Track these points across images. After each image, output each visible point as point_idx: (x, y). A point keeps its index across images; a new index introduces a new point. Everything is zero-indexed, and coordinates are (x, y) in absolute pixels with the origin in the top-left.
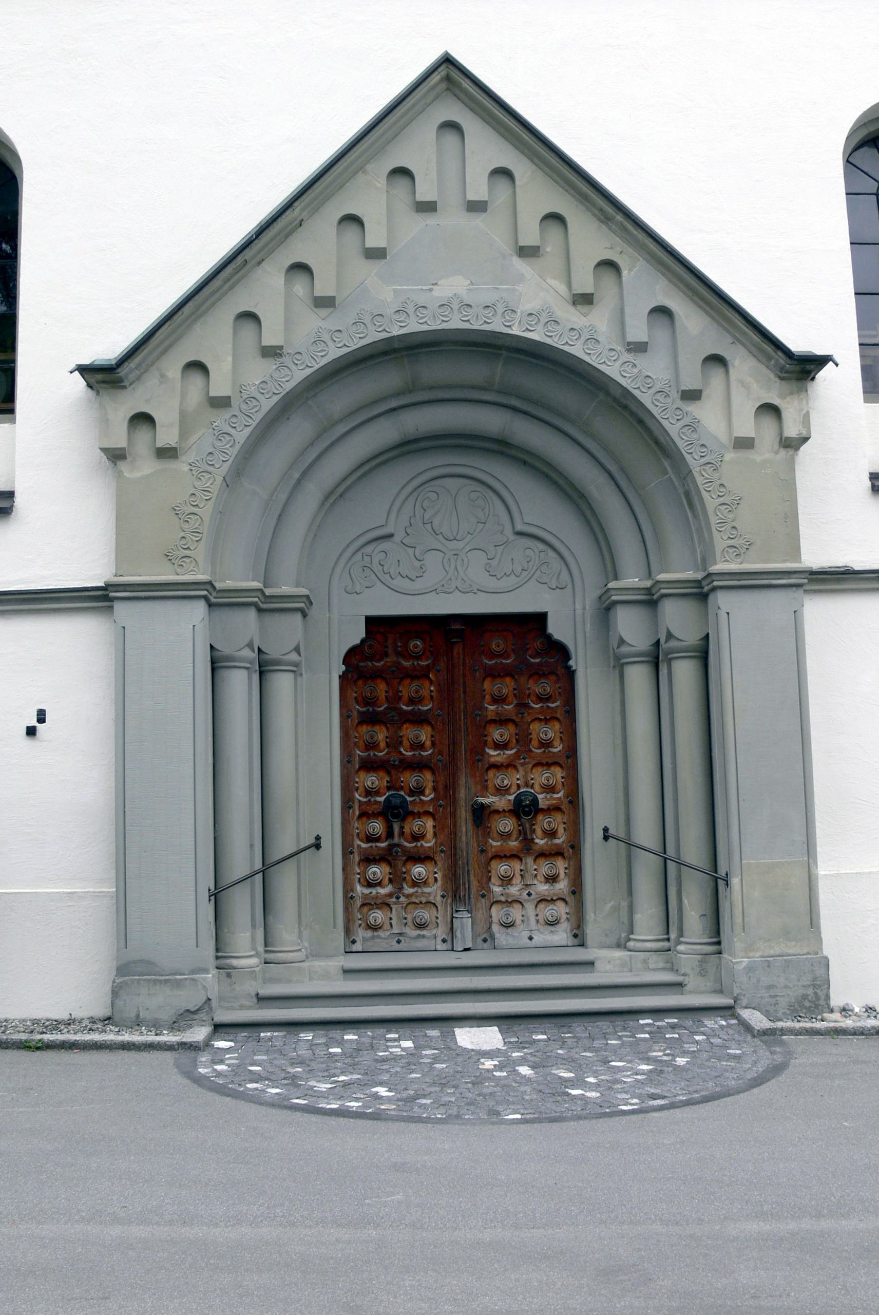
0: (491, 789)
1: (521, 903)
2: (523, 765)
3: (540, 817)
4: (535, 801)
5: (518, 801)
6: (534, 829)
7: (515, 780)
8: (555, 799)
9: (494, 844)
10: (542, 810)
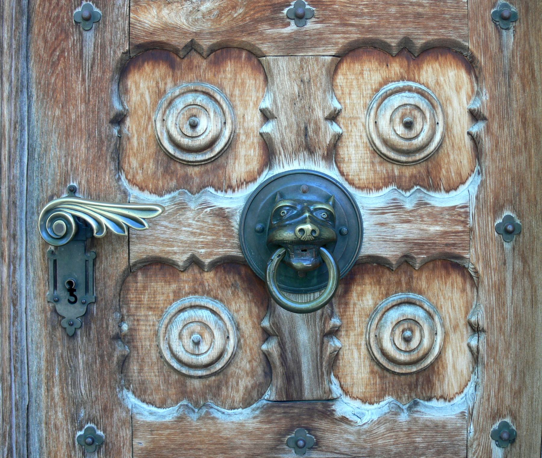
0: (139, 158)
1: (187, 351)
2: (293, 47)
3: (365, 297)
4: (340, 228)
5: (265, 219)
6: (336, 356)
7: (253, 119)
8: (435, 216)
9: (146, 413)
10: (378, 263)
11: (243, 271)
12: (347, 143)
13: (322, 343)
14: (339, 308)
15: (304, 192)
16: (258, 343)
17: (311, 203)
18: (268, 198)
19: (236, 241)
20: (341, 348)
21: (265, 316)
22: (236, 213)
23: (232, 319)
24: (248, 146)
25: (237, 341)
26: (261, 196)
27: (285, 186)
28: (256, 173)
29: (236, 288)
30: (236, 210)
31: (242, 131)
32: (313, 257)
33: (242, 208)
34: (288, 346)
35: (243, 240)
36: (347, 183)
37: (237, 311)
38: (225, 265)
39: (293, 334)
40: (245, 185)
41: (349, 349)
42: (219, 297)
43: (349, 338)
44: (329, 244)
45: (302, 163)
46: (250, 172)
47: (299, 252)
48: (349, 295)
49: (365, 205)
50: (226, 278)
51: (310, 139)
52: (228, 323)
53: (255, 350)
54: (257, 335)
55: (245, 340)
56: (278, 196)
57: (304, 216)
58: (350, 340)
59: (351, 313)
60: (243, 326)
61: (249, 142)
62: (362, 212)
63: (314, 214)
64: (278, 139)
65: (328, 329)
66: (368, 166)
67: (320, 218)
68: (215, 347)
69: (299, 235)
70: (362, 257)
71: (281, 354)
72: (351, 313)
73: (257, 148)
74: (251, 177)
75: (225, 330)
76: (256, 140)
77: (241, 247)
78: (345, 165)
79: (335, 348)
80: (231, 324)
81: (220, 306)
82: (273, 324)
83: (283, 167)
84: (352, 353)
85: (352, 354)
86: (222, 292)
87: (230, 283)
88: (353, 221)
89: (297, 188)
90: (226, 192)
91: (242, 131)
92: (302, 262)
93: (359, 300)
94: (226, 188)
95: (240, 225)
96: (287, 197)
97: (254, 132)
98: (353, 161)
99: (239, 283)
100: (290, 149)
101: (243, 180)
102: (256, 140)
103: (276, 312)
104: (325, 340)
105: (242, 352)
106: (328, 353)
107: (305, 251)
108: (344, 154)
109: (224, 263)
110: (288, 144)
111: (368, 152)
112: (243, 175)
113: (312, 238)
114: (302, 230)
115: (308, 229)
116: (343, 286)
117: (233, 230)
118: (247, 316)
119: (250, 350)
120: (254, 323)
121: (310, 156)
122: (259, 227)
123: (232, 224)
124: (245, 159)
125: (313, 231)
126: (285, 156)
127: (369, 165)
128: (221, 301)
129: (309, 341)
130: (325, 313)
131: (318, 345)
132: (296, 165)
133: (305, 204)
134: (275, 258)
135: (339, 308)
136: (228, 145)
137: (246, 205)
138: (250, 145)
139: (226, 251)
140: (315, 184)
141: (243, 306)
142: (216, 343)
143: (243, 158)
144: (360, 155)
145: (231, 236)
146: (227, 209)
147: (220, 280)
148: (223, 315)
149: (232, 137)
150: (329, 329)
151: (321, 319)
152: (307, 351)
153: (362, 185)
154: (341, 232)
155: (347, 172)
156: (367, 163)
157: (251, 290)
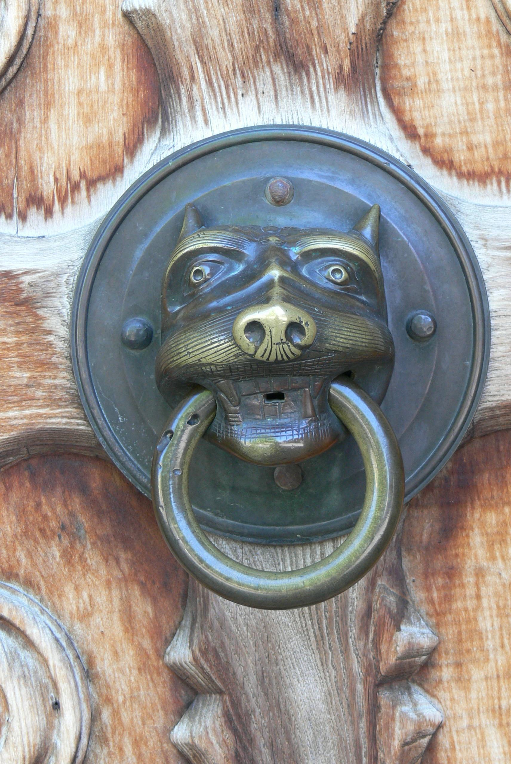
11: (95, 479)
12: (422, 26)
13: (374, 708)
14: (428, 589)
15: (279, 202)
16: (160, 719)
17: (293, 235)
18: (158, 229)
19: (63, 379)
20: (440, 726)
21: (178, 626)
22: (59, 285)
23: (68, 641)
24: (86, 59)
25: (86, 716)
26: (137, 222)
27: (214, 187)
28: (119, 149)
29: (74, 537)
30: (57, 275)
31: (63, 11)
32: (305, 417)
33: (76, 269)
34: (259, 723)
35: (85, 375)
36: (428, 161)
37: (85, 616)
38: (34, 462)
39: (271, 683)
40: (84, 193)
41: (470, 727)
42: (22, 572)
43: (467, 689)
44: (361, 369)
45: (268, 105)
46: (100, 146)
47: (257, 401)
48: (460, 540)
49: (493, 233)
50: (38, 505)
51: (292, 21)
52: (54, 659)
53: (151, 743)
54: (154, 693)
55: (116, 714)
56: (190, 221)
57: (264, 279)
58: (473, 695)
59: (471, 604)
60: (105, 665)
61: (90, 45)
62: (482, 256)
63: (304, 271)
64: (183, 27)
65: (390, 660)
66: (497, 101)
67: (324, 283)
68: (11, 739)
69: (247, 342)
70: (492, 409)
71: (237, 755)
72: (471, 604)
73: (118, 65)
74: (104, 162)
75: (46, 680)
76: (113, 37)
77: (79, 400)
78: (418, 103)
79: (419, 724)
80: (65, 660)
81: (24, 600)
82: (204, 652)
83: (206, 122)
84: (483, 739)
85: (483, 742)
86: (29, 555)
87: (53, 524)
88: (452, 291)
89: (258, 187)
90: (23, 217)
91: (63, 11)
92: (269, 435)
93: (493, 558)
94: (22, 206)
95: (73, 326)
96: (222, 220)
97: (103, 12)
98: (445, 86)
99: (84, 520)
100: (226, 58)
101: (76, 175)
102: (112, 38)
103: (212, 613)
104: (385, 697)
105: (110, 754)
106: (396, 743)
107: (279, 396)
108: (413, 64)
109: (31, 457)
110: (218, 41)
111: (496, 51)
112: (76, 157)
113: (290, 350)
114: (255, 327)
115: (277, 320)
116: (435, 511)
117: (50, 345)
118: (117, 629)
119: (136, 744)
120: (141, 651)
121: (294, 78)
122: (133, 328)
123: (46, 325)
124: (80, 104)
125: (294, 327)
126: (210, 83)
127: (501, 94)
128: (29, 583)
129: (328, 702)
130: (376, 606)
131: (360, 716)
132: (248, 113)
133: (273, 240)
134: (182, 428)
135: (428, 589)
136: (18, 61)
137: (88, 257)
138: (93, 57)
139: (31, 417)
140: (313, 172)
141: (101, 598)
142: (15, 725)
143: (73, 101)
144: (467, 64)
145: (45, 365)
146: (25, 273)
147: (21, 513)
148: (34, 632)
149: (30, 32)
150: (393, 660)
151: (364, 629)
152: (326, 740)
153: (479, 167)
154: (411, 331)
155: (427, 127)
156: (495, 88)
157: (126, 543)
